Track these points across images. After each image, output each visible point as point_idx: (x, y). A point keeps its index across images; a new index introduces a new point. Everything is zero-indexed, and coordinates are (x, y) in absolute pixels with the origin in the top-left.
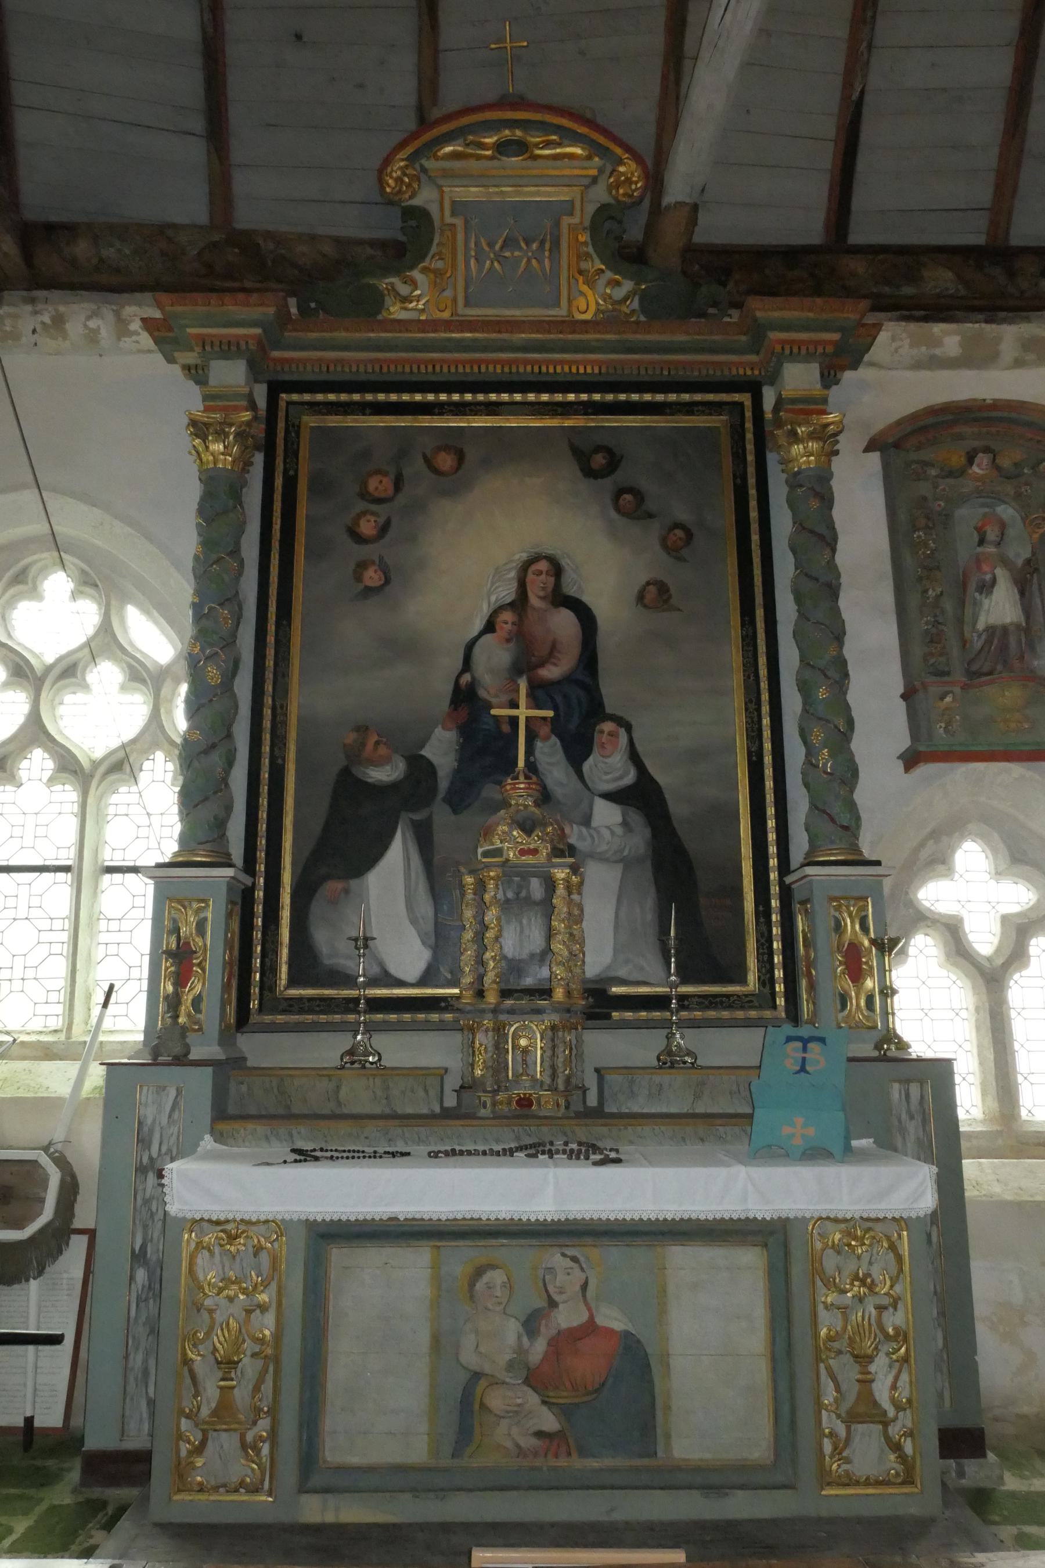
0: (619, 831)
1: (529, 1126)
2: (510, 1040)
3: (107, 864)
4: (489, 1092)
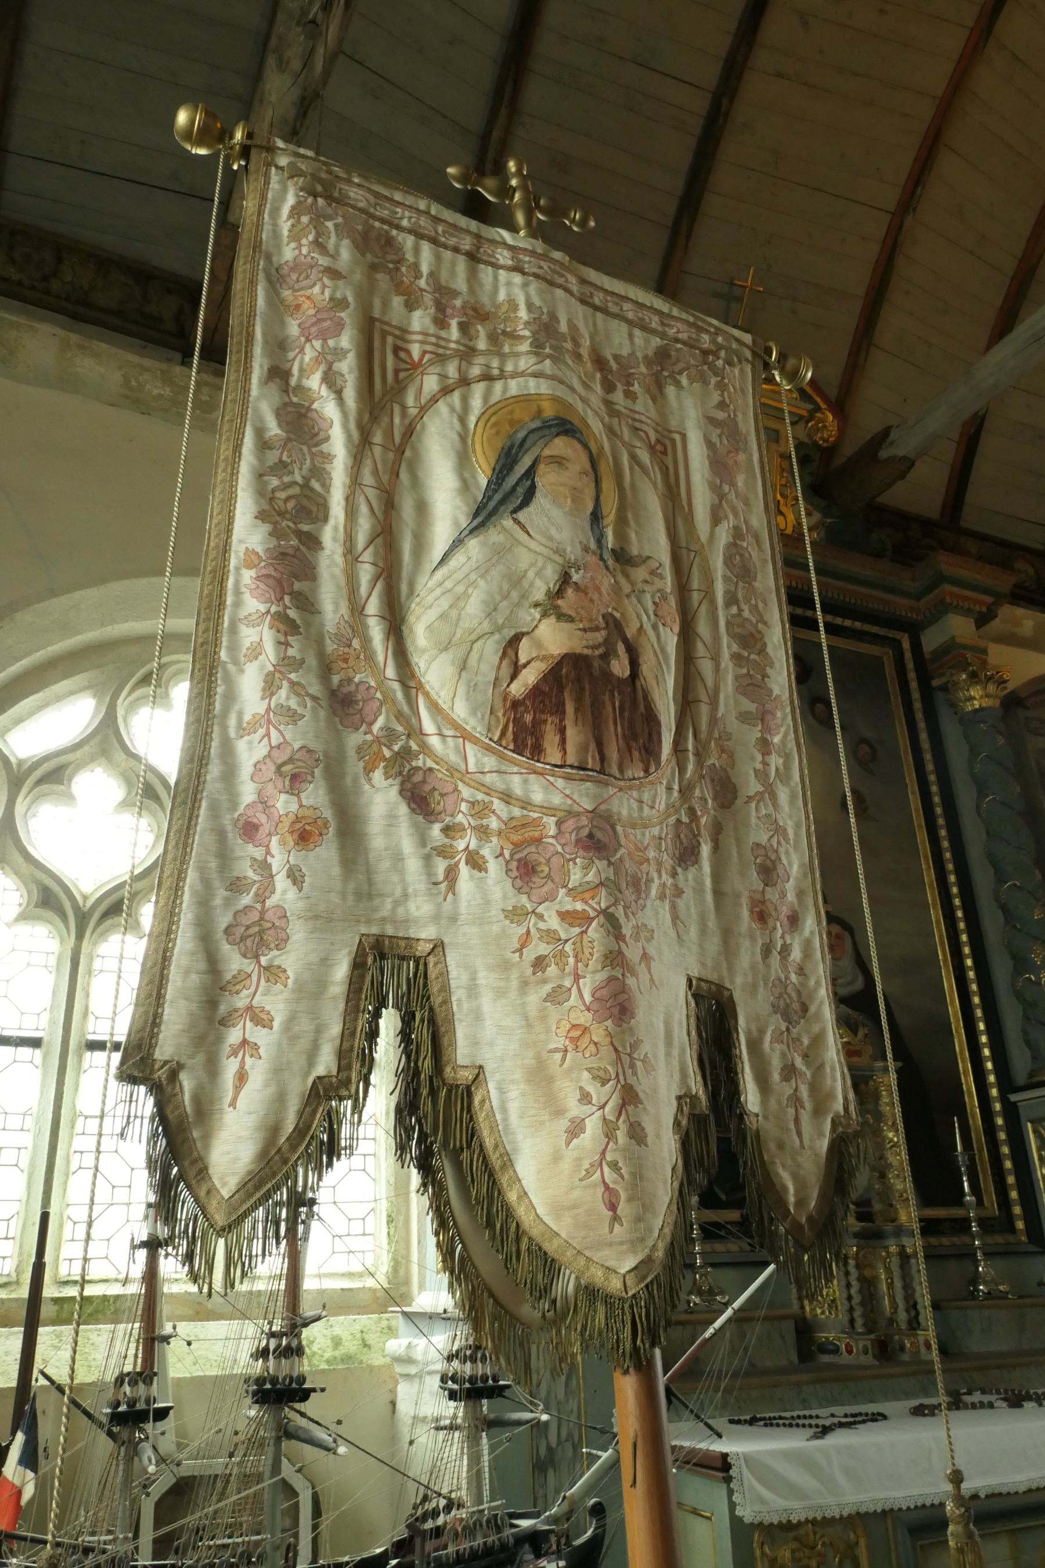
3: (91, 1037)
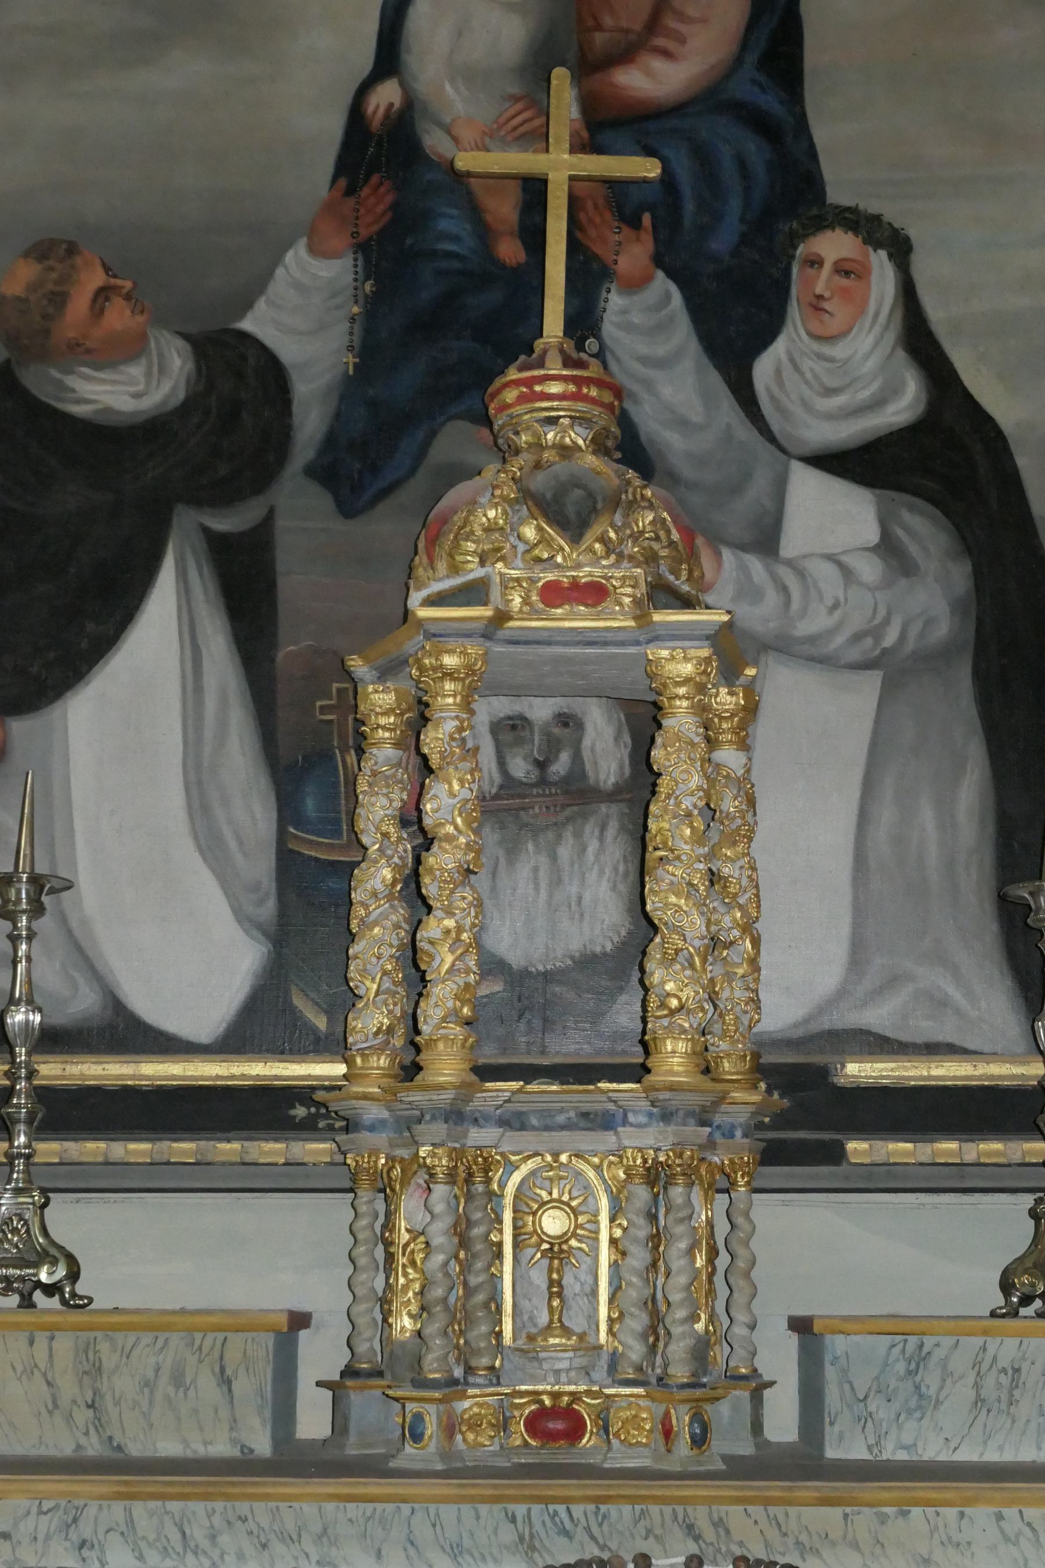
0: (869, 569)
1: (566, 1500)
2: (508, 1216)
4: (434, 1385)
